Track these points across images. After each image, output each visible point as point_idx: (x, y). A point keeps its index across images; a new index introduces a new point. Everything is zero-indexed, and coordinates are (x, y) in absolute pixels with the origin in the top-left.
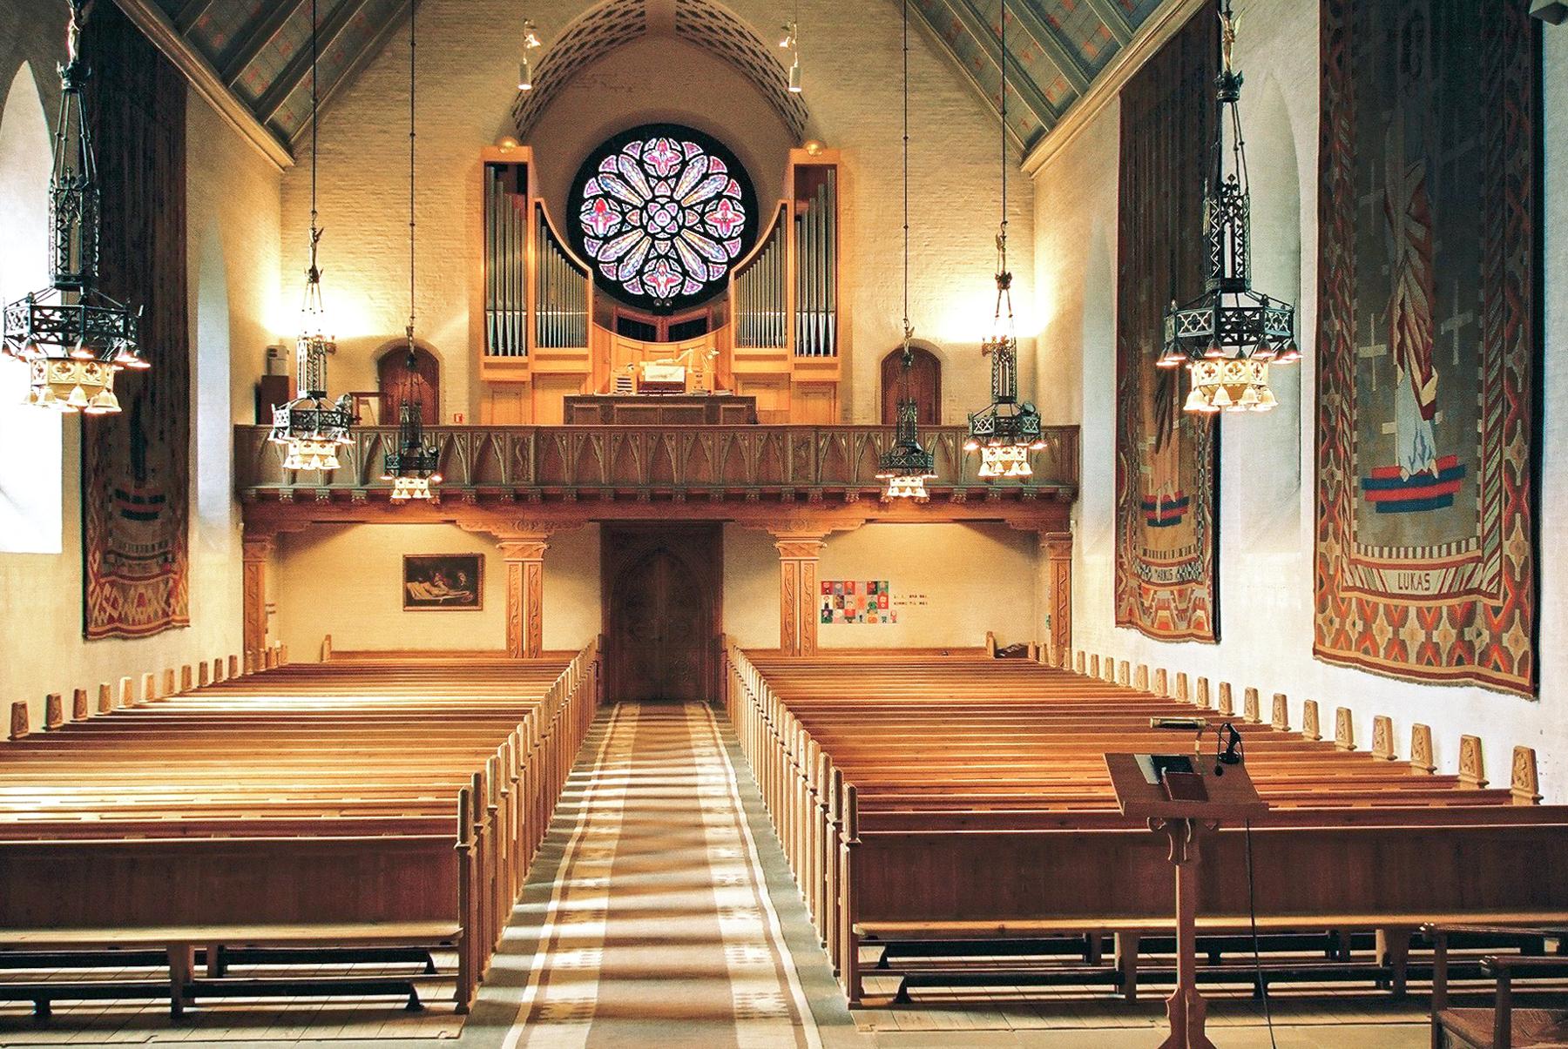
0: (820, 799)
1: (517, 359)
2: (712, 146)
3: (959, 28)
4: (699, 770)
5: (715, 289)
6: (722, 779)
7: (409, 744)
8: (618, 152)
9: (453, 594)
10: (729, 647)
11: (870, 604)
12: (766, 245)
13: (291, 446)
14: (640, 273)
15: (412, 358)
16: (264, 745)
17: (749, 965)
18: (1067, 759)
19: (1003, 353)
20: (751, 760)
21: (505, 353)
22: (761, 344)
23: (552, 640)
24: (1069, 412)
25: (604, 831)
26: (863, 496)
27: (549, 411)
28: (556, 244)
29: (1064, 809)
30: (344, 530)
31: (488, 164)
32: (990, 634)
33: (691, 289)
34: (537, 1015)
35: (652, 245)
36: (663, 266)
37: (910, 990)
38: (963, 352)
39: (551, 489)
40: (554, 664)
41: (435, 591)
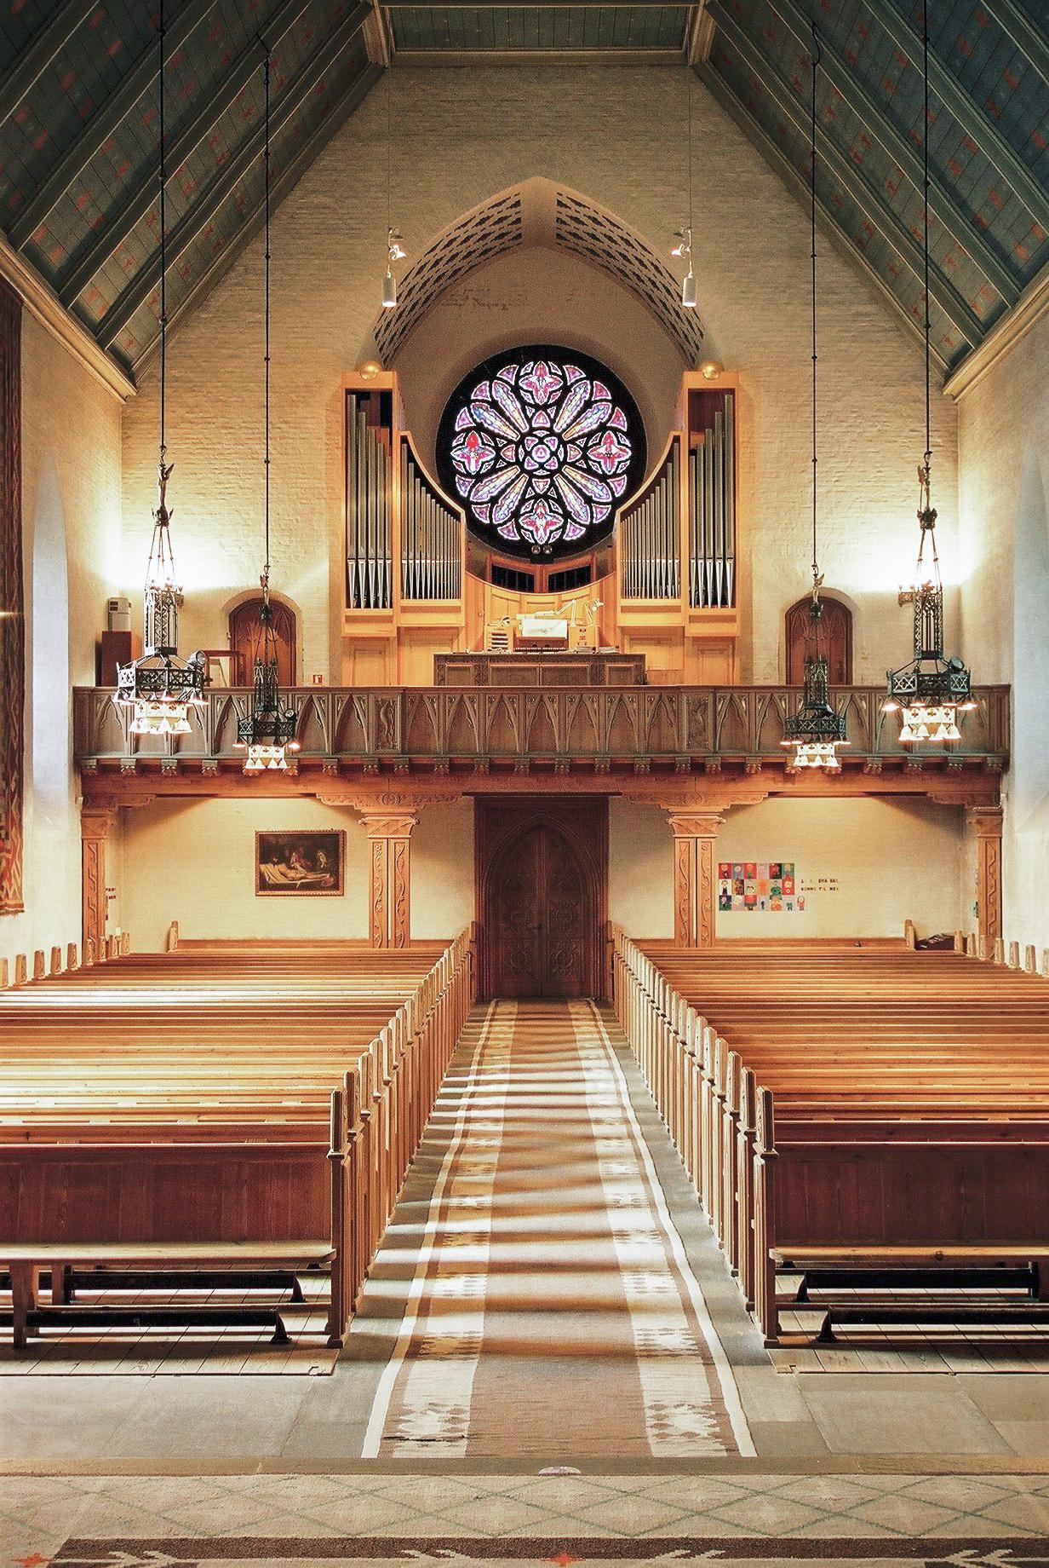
0: (729, 1106)
1: (380, 612)
2: (596, 370)
3: (871, 230)
4: (585, 1075)
5: (599, 533)
6: (612, 1087)
8: (492, 378)
10: (615, 935)
11: (773, 890)
12: (657, 482)
13: (137, 708)
14: (516, 515)
15: (267, 611)
16: (110, 1042)
17: (650, 1297)
18: (1006, 1063)
19: (927, 602)
20: (643, 1063)
21: (376, 606)
23: (420, 929)
24: (998, 672)
25: (483, 1142)
26: (766, 766)
28: (424, 482)
29: (1004, 1119)
31: (349, 392)
32: (909, 923)
33: (574, 534)
34: (417, 1350)
35: (529, 484)
37: (835, 1328)
38: (878, 606)
39: (422, 759)
41: (292, 874)
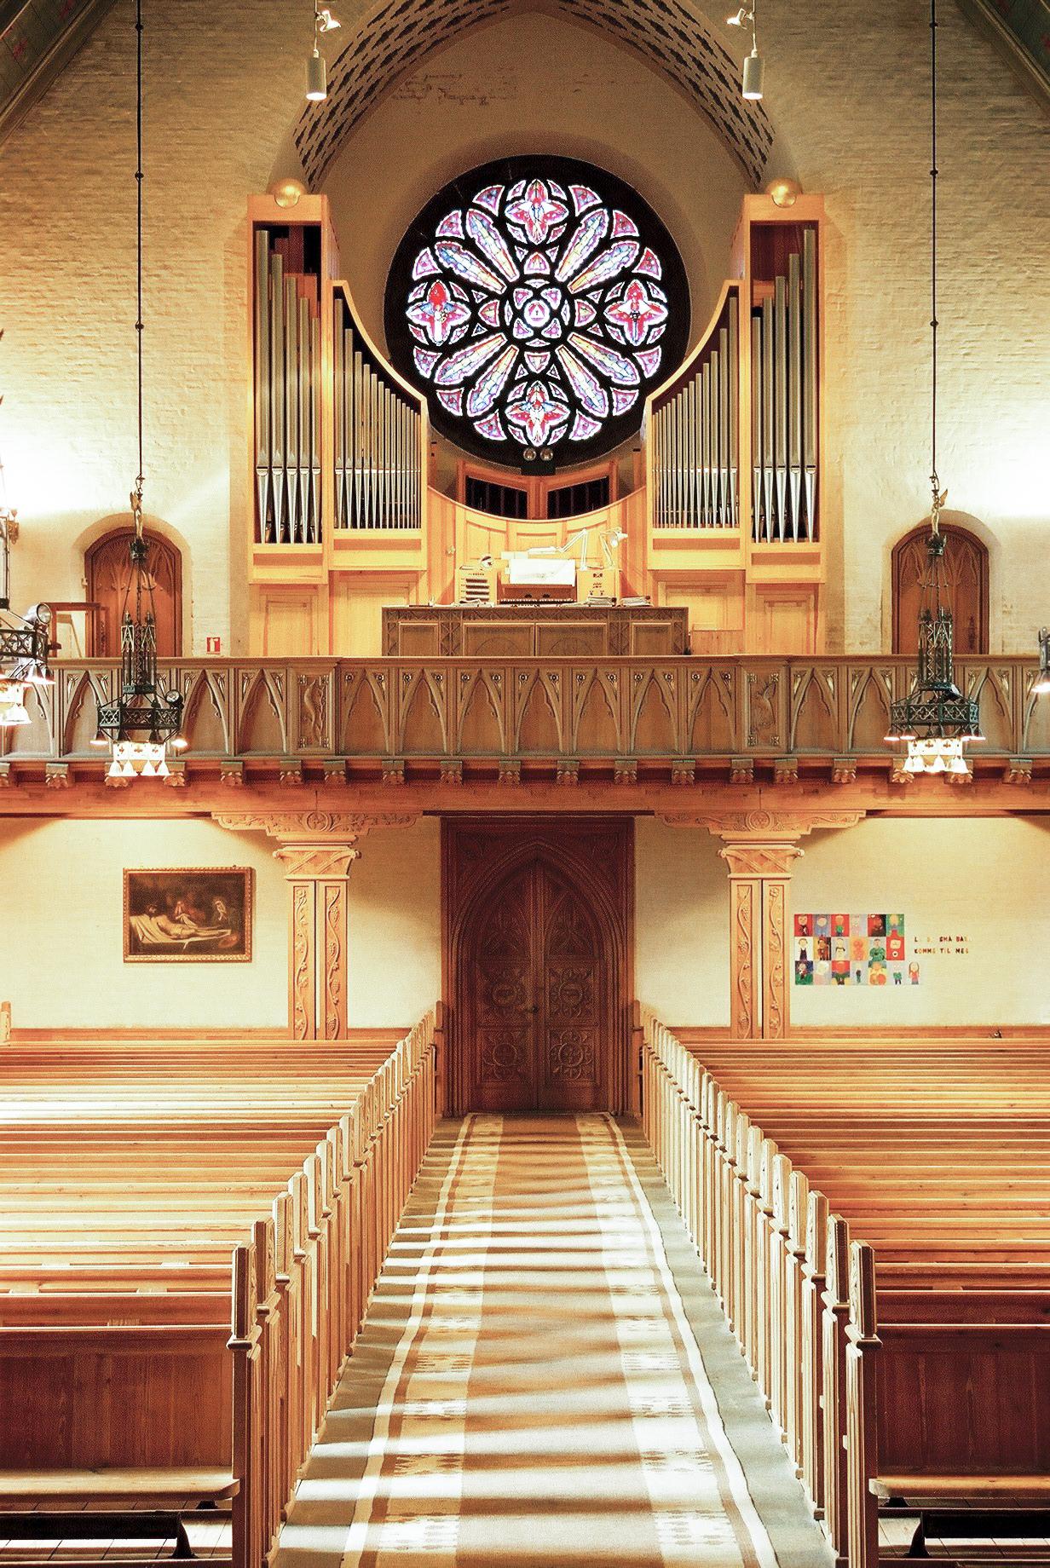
0: (810, 1269)
1: (304, 548)
2: (618, 194)
5: (620, 430)
6: (640, 1241)
7: (140, 1178)
9: (205, 934)
11: (874, 953)
12: (704, 357)
14: (500, 403)
15: (140, 548)
20: (685, 1209)
22: (696, 521)
25: (453, 1324)
26: (862, 772)
27: (359, 633)
28: (368, 358)
30: (34, 827)
31: (259, 226)
33: (585, 430)
36: (538, 392)
39: (363, 762)
40: (367, 1052)
41: (176, 929)
